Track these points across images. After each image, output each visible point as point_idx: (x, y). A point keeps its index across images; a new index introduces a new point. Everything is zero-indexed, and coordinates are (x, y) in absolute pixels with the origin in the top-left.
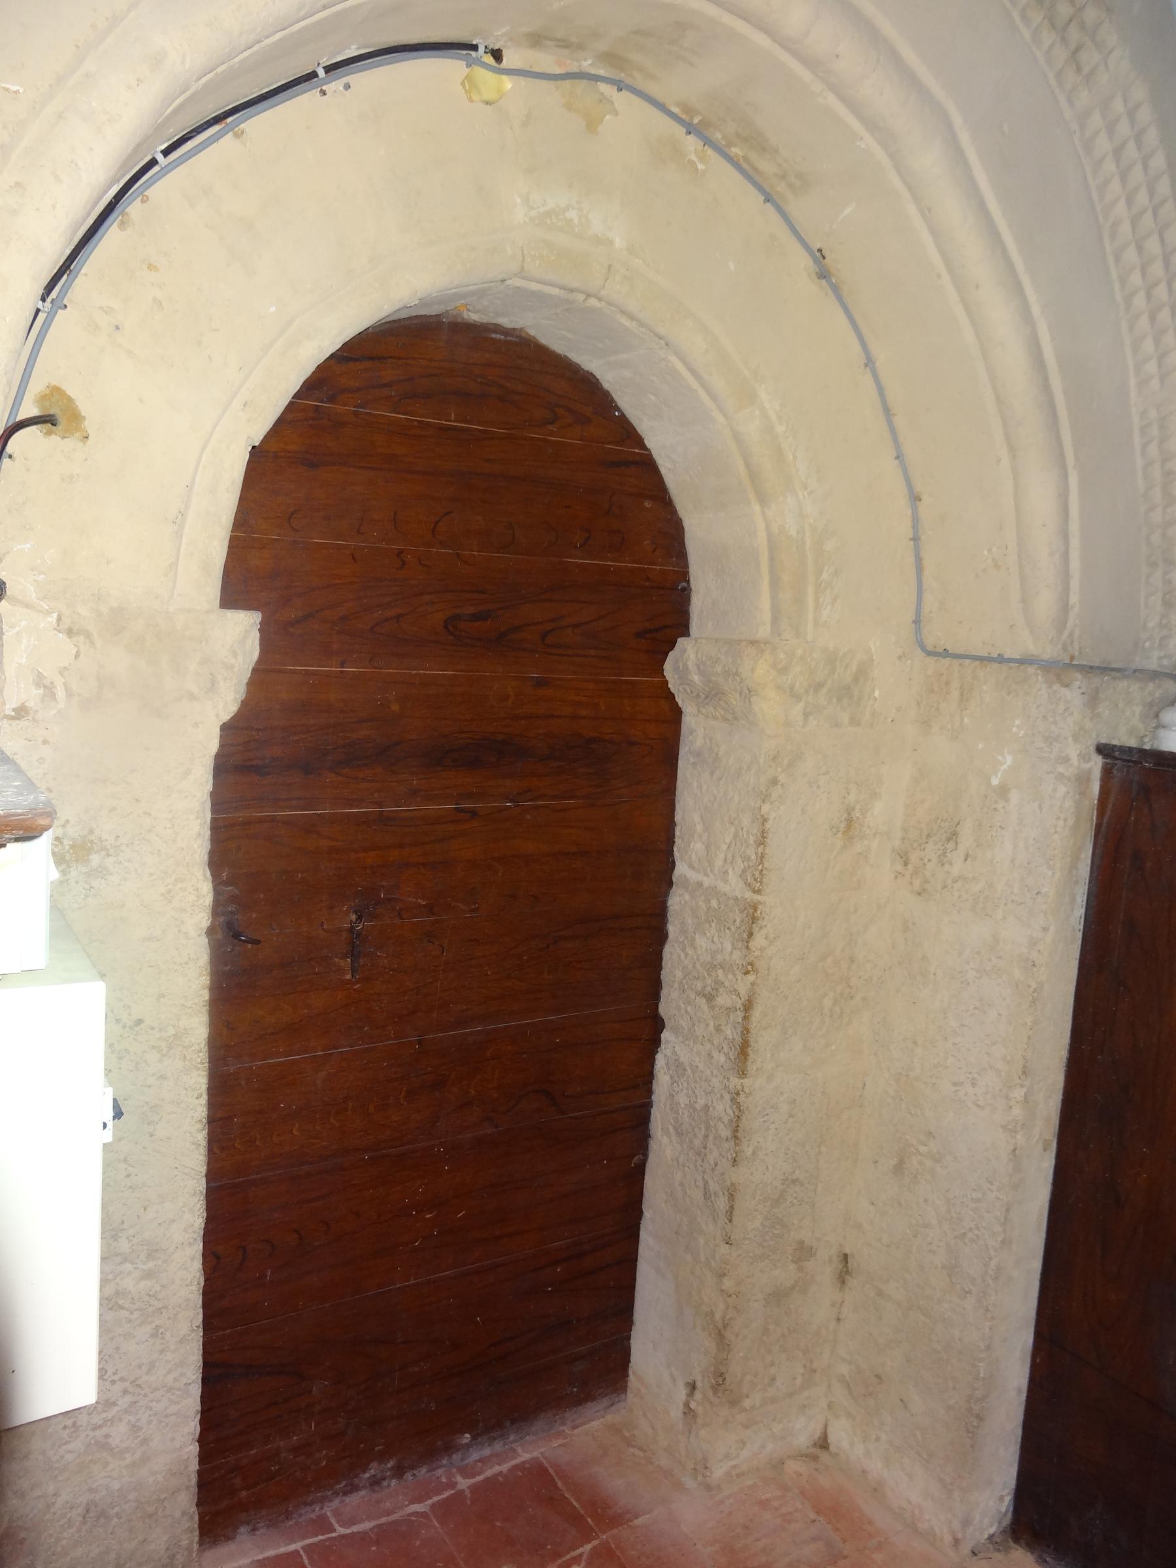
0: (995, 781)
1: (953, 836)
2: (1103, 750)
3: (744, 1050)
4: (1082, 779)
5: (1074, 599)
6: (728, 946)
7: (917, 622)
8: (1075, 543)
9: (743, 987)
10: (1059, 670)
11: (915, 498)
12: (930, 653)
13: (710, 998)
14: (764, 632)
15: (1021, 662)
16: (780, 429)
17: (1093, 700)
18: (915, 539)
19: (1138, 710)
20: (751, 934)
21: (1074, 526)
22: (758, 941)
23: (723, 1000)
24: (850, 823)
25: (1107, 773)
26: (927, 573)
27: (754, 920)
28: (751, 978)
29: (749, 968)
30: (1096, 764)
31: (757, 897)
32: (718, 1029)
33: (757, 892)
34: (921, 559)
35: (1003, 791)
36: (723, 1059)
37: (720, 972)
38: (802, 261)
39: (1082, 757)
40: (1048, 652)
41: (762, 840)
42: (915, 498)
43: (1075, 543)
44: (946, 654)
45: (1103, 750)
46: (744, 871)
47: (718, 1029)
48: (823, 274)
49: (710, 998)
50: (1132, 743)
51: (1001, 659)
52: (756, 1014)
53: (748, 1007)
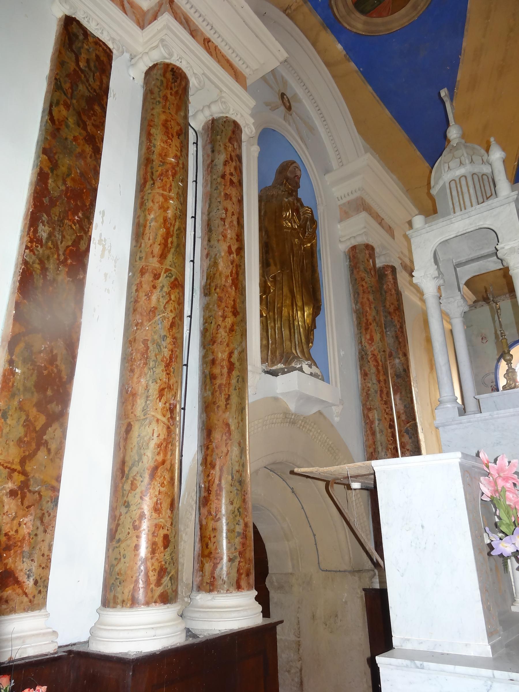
0: (344, 600)
1: (336, 616)
2: (364, 590)
3: (301, 683)
4: (362, 597)
5: (351, 556)
6: (292, 655)
7: (319, 563)
8: (349, 544)
9: (299, 665)
10: (353, 572)
11: (314, 535)
12: (323, 571)
13: (289, 672)
14: (290, 571)
15: (345, 571)
16: (290, 525)
17: (360, 578)
18: (316, 544)
19: (368, 579)
20: (299, 650)
21: (349, 540)
22: (301, 651)
23: (293, 671)
24: (313, 616)
25: (366, 594)
26: (319, 551)
27: (299, 645)
28: (300, 662)
29: (300, 659)
30: (363, 593)
31: (299, 639)
32: (293, 680)
33: (299, 638)
34: (182, 456)
35: (346, 602)
36: (295, 689)
37: (291, 663)
38: (290, 490)
39: (361, 592)
40: (349, 569)
41: (298, 623)
42: (314, 535)
43: (349, 544)
44: (327, 571)
45: (364, 590)
46: (294, 633)
47: (293, 680)
48: (293, 492)
49: (289, 672)
50: (368, 587)
51: (340, 571)
52: (303, 671)
53: (301, 670)
